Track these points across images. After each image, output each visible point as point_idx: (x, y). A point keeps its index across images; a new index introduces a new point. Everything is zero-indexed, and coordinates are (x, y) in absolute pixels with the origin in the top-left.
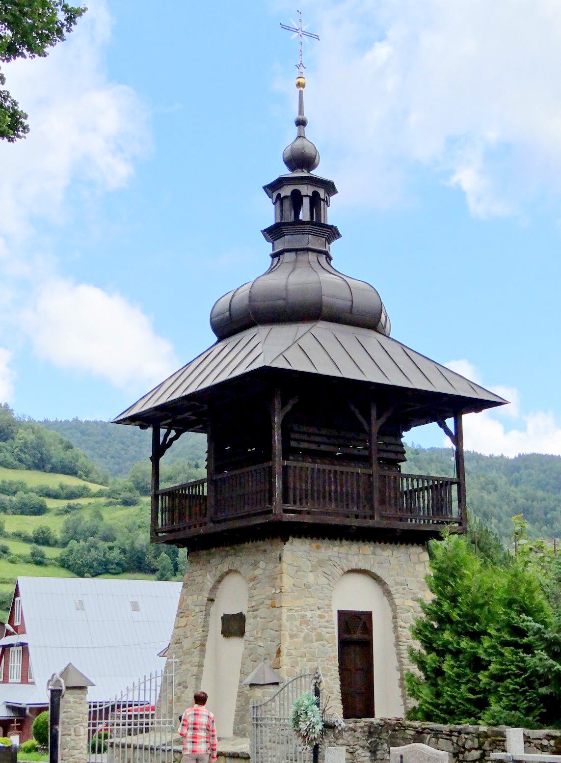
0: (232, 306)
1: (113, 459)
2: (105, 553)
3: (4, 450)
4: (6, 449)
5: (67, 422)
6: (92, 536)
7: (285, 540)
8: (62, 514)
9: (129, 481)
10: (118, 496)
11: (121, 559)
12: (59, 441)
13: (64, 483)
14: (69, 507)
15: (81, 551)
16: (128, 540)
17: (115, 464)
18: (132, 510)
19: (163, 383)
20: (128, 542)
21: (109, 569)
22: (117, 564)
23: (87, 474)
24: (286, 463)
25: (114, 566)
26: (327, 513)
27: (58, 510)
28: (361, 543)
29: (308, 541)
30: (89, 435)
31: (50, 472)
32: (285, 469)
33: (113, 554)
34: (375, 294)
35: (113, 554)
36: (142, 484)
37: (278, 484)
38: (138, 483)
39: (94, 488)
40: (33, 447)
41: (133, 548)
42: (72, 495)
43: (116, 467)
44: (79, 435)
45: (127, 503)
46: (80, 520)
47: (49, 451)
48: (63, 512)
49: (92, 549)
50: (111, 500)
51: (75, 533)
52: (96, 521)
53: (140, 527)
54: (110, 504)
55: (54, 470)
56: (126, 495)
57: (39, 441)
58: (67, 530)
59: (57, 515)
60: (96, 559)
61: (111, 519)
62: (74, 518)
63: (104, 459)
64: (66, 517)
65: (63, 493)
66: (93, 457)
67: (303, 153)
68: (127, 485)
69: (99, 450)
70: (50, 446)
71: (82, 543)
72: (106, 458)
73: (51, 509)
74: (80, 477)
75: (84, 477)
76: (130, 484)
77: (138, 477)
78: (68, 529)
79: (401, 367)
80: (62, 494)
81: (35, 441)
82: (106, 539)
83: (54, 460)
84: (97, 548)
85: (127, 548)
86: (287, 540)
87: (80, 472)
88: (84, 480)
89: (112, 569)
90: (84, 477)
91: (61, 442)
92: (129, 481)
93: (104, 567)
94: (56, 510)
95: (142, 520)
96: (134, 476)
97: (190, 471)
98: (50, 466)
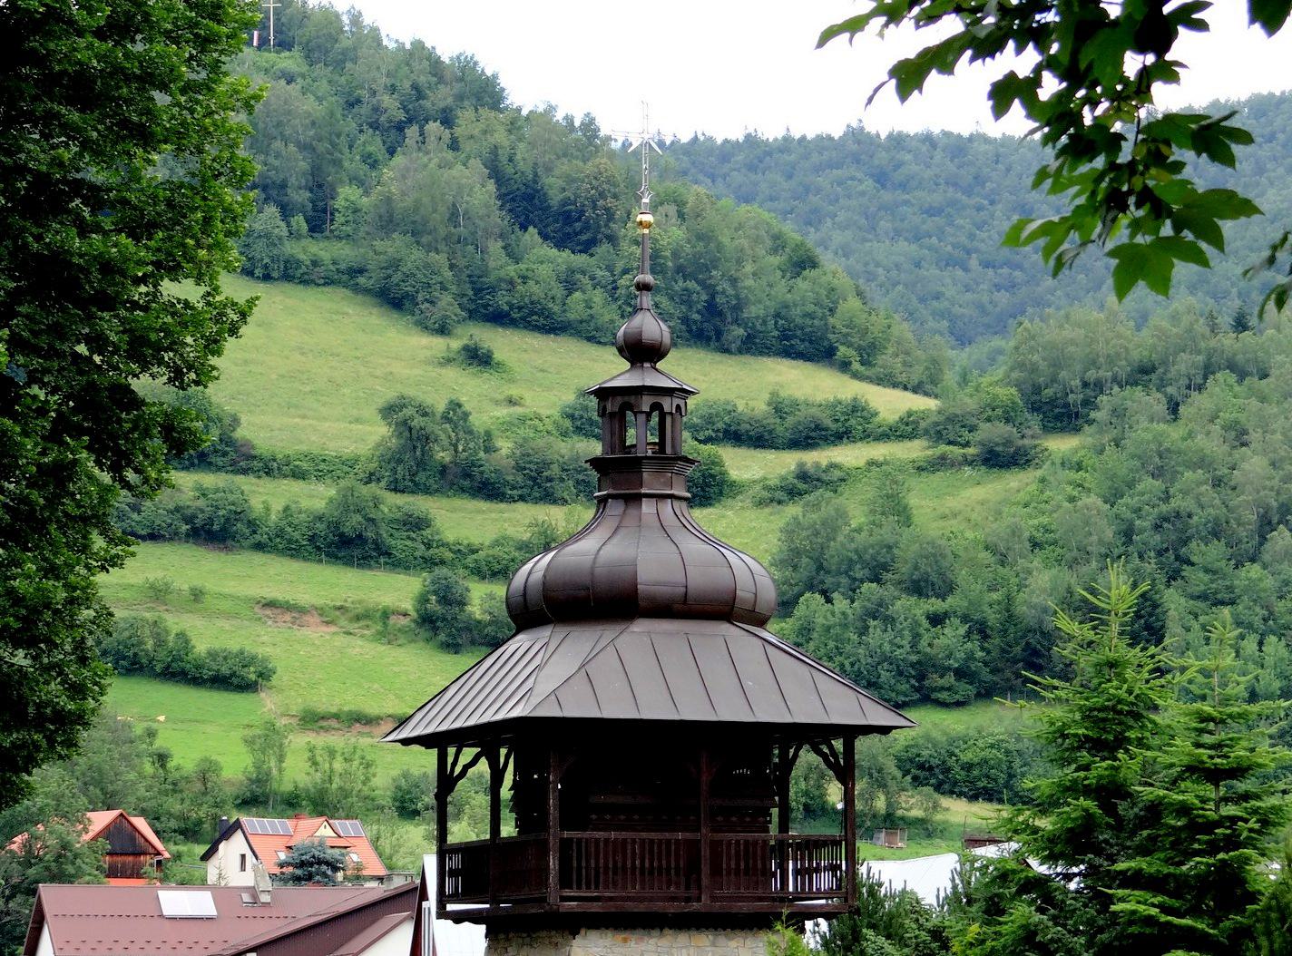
0: (528, 592)
1: (990, 272)
2: (916, 637)
3: (585, 280)
4: (592, 278)
5: (824, 142)
6: (876, 579)
7: (574, 933)
8: (780, 502)
9: (1006, 381)
10: (967, 436)
11: (970, 657)
12: (769, 243)
13: (784, 394)
14: (803, 476)
15: (838, 630)
16: (992, 589)
17: (998, 287)
18: (1016, 482)
19: (446, 689)
20: (995, 596)
21: (935, 690)
22: (961, 673)
23: (868, 353)
24: (566, 834)
25: (950, 679)
26: (629, 899)
27: (768, 488)
28: (693, 933)
29: (610, 933)
30: (903, 186)
31: (740, 352)
32: (565, 845)
33: (942, 641)
34: (727, 570)
35: (942, 641)
36: (1048, 392)
37: (553, 863)
38: (1037, 390)
39: (889, 403)
40: (680, 270)
41: (1010, 618)
42: (809, 437)
43: (1003, 298)
44: (869, 184)
45: (998, 459)
46: (830, 527)
47: (734, 281)
48: (780, 495)
49: (872, 623)
50: (943, 448)
51: (820, 568)
52: (886, 533)
53: (1035, 545)
54: (940, 464)
55: (753, 345)
56: (993, 432)
57: (700, 246)
58: (790, 559)
59: (761, 503)
60: (886, 658)
61: (944, 517)
62: (815, 516)
63: (959, 273)
64: (793, 510)
65: (782, 429)
66: (918, 265)
67: (640, 341)
68: (995, 397)
69: (940, 240)
70: (739, 262)
71: (841, 603)
72: (966, 270)
73: (733, 484)
74: (845, 366)
75: (856, 366)
76: (1007, 393)
77: (1034, 369)
78: (797, 552)
79: (748, 684)
80: (780, 430)
81: (688, 248)
82: (918, 588)
83: (753, 311)
84: (889, 621)
85: (993, 618)
86: (578, 933)
87: (843, 351)
88: (856, 376)
89: (943, 689)
90: (856, 366)
91: (778, 243)
92: (1006, 381)
93: (913, 681)
94: (758, 487)
95: (1045, 520)
96: (1021, 366)
97: (1213, 343)
98: (741, 332)
